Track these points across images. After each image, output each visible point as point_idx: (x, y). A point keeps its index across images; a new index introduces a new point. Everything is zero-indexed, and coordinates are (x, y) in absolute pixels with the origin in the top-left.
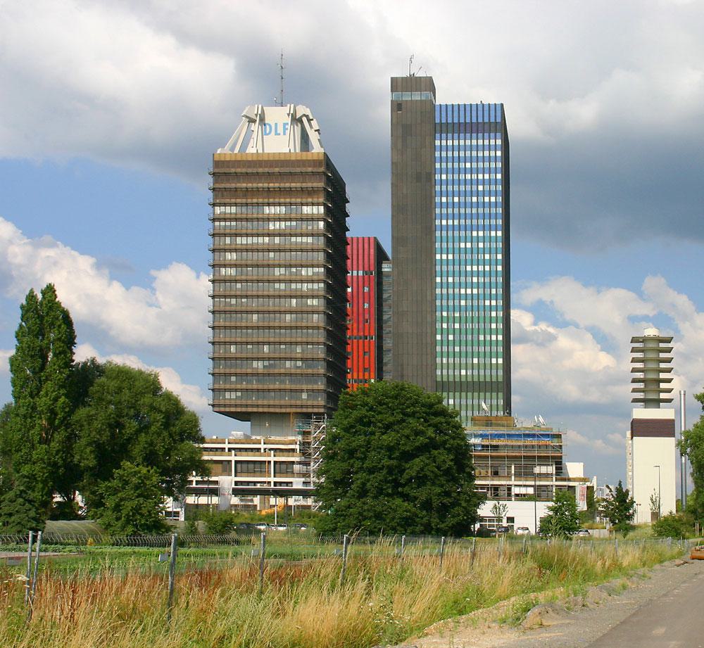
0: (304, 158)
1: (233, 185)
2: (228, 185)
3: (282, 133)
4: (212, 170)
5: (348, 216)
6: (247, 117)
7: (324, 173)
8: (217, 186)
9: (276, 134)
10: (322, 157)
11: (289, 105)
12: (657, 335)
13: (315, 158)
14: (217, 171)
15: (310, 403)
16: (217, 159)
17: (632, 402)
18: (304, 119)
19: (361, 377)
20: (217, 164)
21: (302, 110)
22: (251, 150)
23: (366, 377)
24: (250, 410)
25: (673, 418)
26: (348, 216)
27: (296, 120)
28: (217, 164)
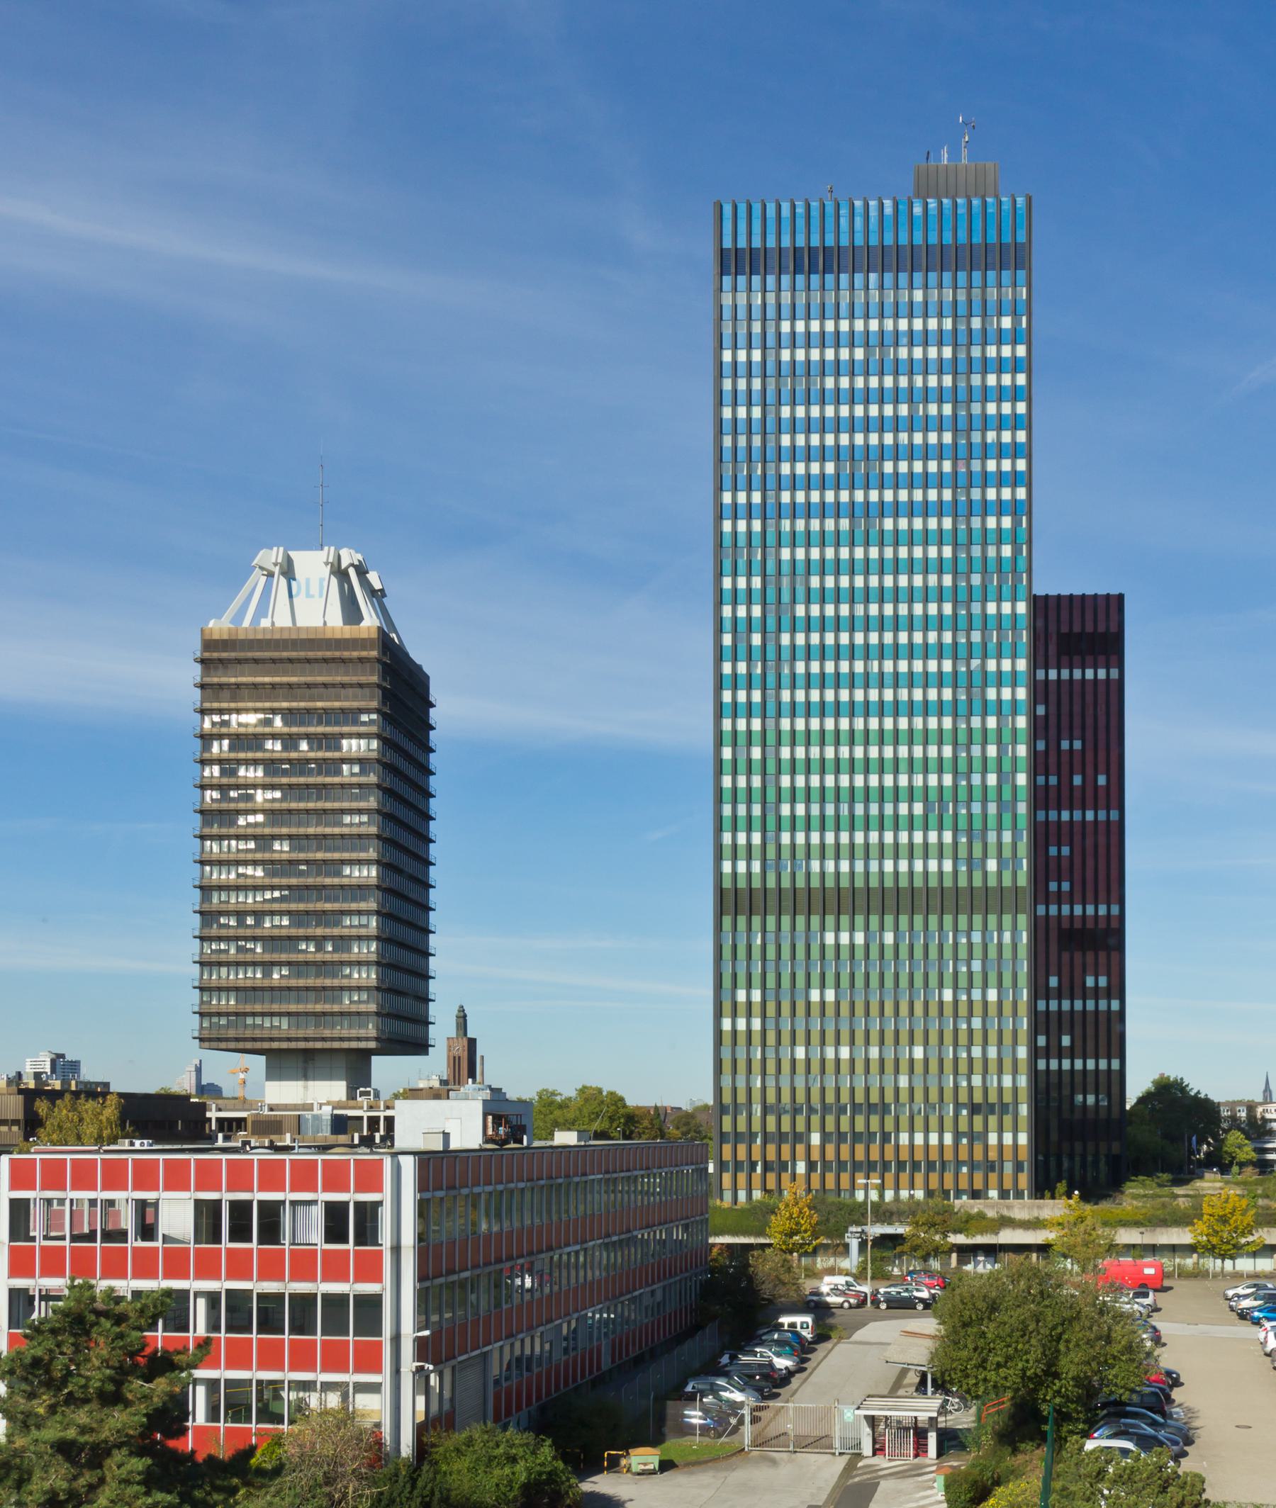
0: (347, 636)
1: (233, 680)
2: (224, 680)
3: (317, 595)
4: (198, 654)
5: (433, 751)
6: (262, 568)
7: (378, 661)
8: (208, 680)
9: (308, 595)
10: (374, 635)
11: (326, 548)
12: (1198, 1184)
13: (366, 636)
14: (207, 655)
15: (293, 1034)
16: (207, 637)
17: (462, 1009)
18: (352, 572)
19: (786, 1127)
20: (209, 644)
21: (349, 557)
22: (265, 623)
23: (978, 1185)
24: (310, 1045)
25: (268, 1083)
26: (433, 751)
27: (340, 574)
28: (209, 644)
